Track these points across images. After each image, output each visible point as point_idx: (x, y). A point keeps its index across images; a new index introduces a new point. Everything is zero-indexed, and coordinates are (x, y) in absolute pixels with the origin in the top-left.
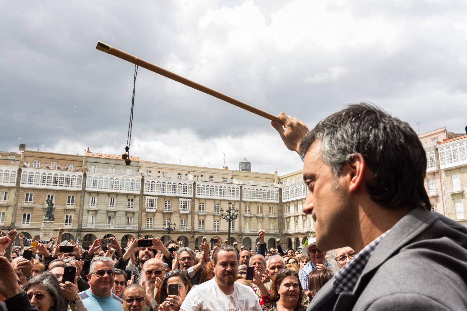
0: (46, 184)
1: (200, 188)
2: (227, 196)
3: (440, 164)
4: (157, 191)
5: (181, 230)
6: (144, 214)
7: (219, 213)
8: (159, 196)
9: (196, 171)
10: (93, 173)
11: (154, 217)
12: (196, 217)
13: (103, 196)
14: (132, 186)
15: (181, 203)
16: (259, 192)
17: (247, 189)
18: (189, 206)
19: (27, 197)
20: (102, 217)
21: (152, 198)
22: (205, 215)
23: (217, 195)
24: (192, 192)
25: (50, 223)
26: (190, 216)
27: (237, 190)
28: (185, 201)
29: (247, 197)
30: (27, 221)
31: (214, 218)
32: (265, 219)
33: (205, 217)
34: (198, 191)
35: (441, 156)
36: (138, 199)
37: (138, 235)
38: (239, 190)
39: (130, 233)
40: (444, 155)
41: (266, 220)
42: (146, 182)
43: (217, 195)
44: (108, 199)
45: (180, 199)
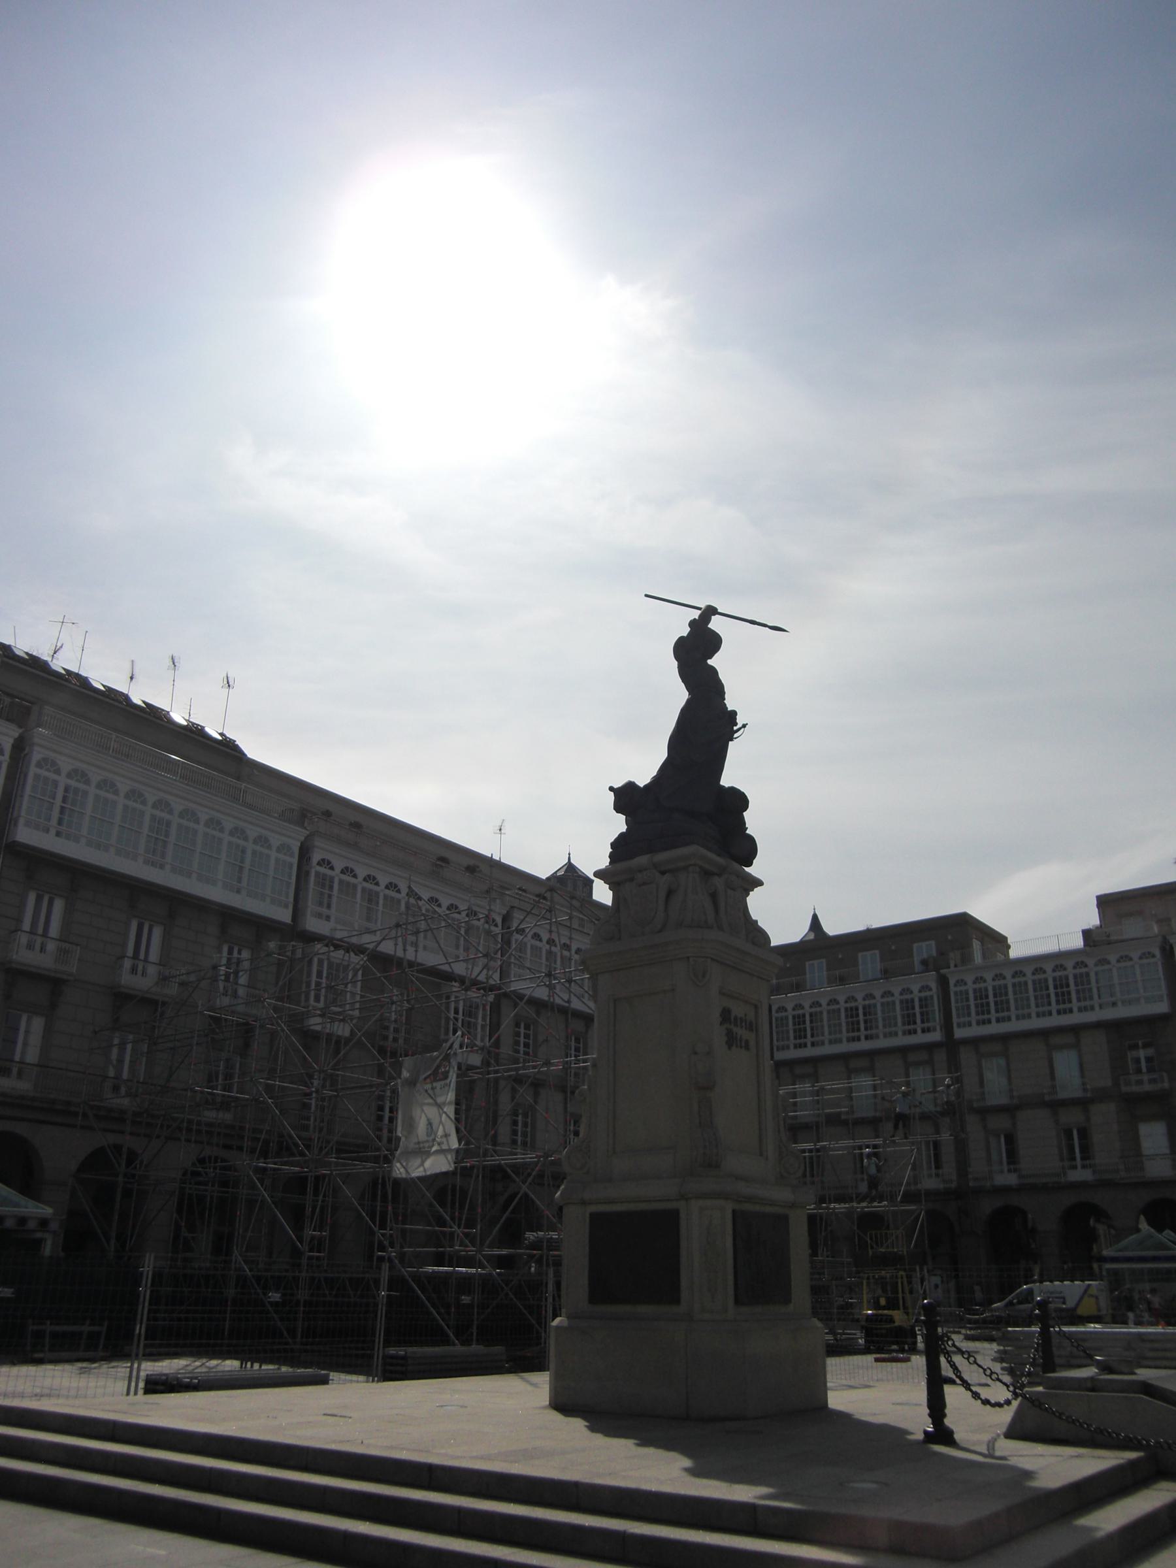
30: (1083, 1159)
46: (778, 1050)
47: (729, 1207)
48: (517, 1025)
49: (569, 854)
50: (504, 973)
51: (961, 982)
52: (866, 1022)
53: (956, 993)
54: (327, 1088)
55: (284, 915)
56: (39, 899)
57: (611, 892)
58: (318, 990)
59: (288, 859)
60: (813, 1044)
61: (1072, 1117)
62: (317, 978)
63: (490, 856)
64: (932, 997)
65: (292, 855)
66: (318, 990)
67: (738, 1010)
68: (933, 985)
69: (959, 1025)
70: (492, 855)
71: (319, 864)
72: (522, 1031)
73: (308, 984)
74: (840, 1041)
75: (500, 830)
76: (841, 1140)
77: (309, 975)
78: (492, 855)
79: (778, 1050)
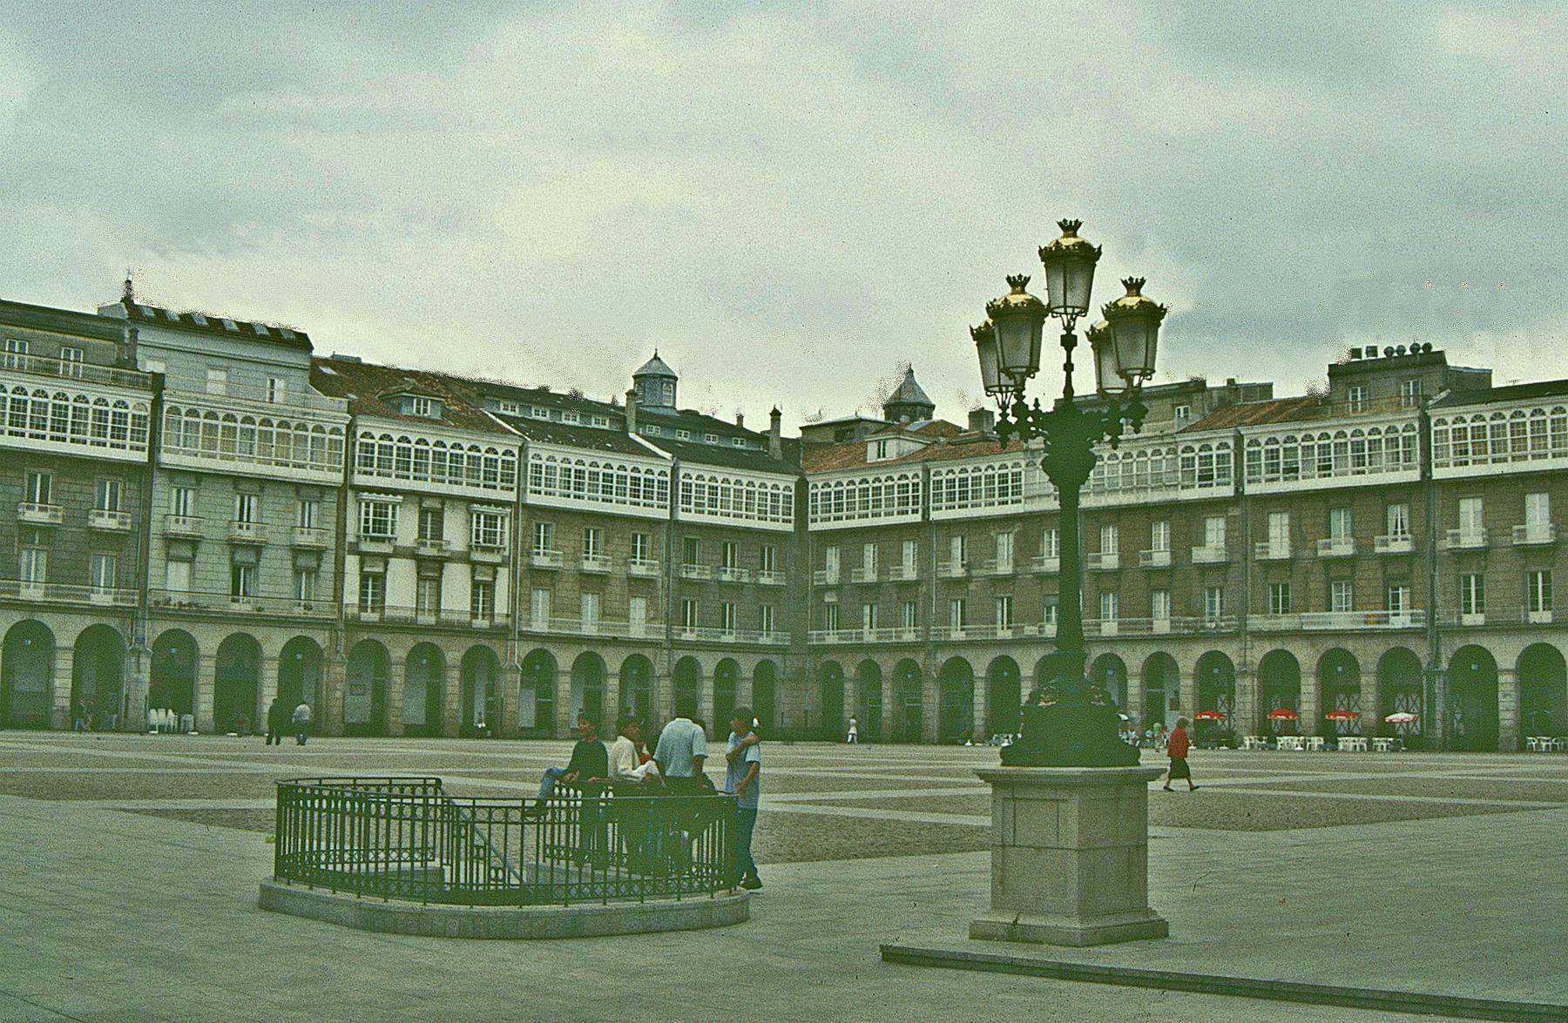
0: (412, 473)
1: (570, 470)
2: (68, 440)
3: (1433, 466)
4: (12, 428)
7: (59, 514)
12: (352, 562)
13: (217, 486)
16: (70, 408)
17: (544, 460)
19: (45, 486)
20: (216, 568)
21: (492, 510)
22: (385, 558)
23: (120, 442)
24: (144, 441)
27: (661, 478)
28: (381, 505)
32: (394, 563)
35: (1436, 442)
36: (331, 500)
38: (668, 479)
40: (1447, 438)
42: (362, 436)
43: (120, 442)
44: (170, 493)
45: (476, 507)
46: (1436, 467)
51: (1442, 422)
52: (1554, 437)
54: (349, 699)
56: (179, 492)
57: (759, 432)
63: (734, 422)
64: (1229, 454)
68: (1231, 443)
69: (933, 509)
70: (740, 418)
76: (607, 844)
78: (740, 418)
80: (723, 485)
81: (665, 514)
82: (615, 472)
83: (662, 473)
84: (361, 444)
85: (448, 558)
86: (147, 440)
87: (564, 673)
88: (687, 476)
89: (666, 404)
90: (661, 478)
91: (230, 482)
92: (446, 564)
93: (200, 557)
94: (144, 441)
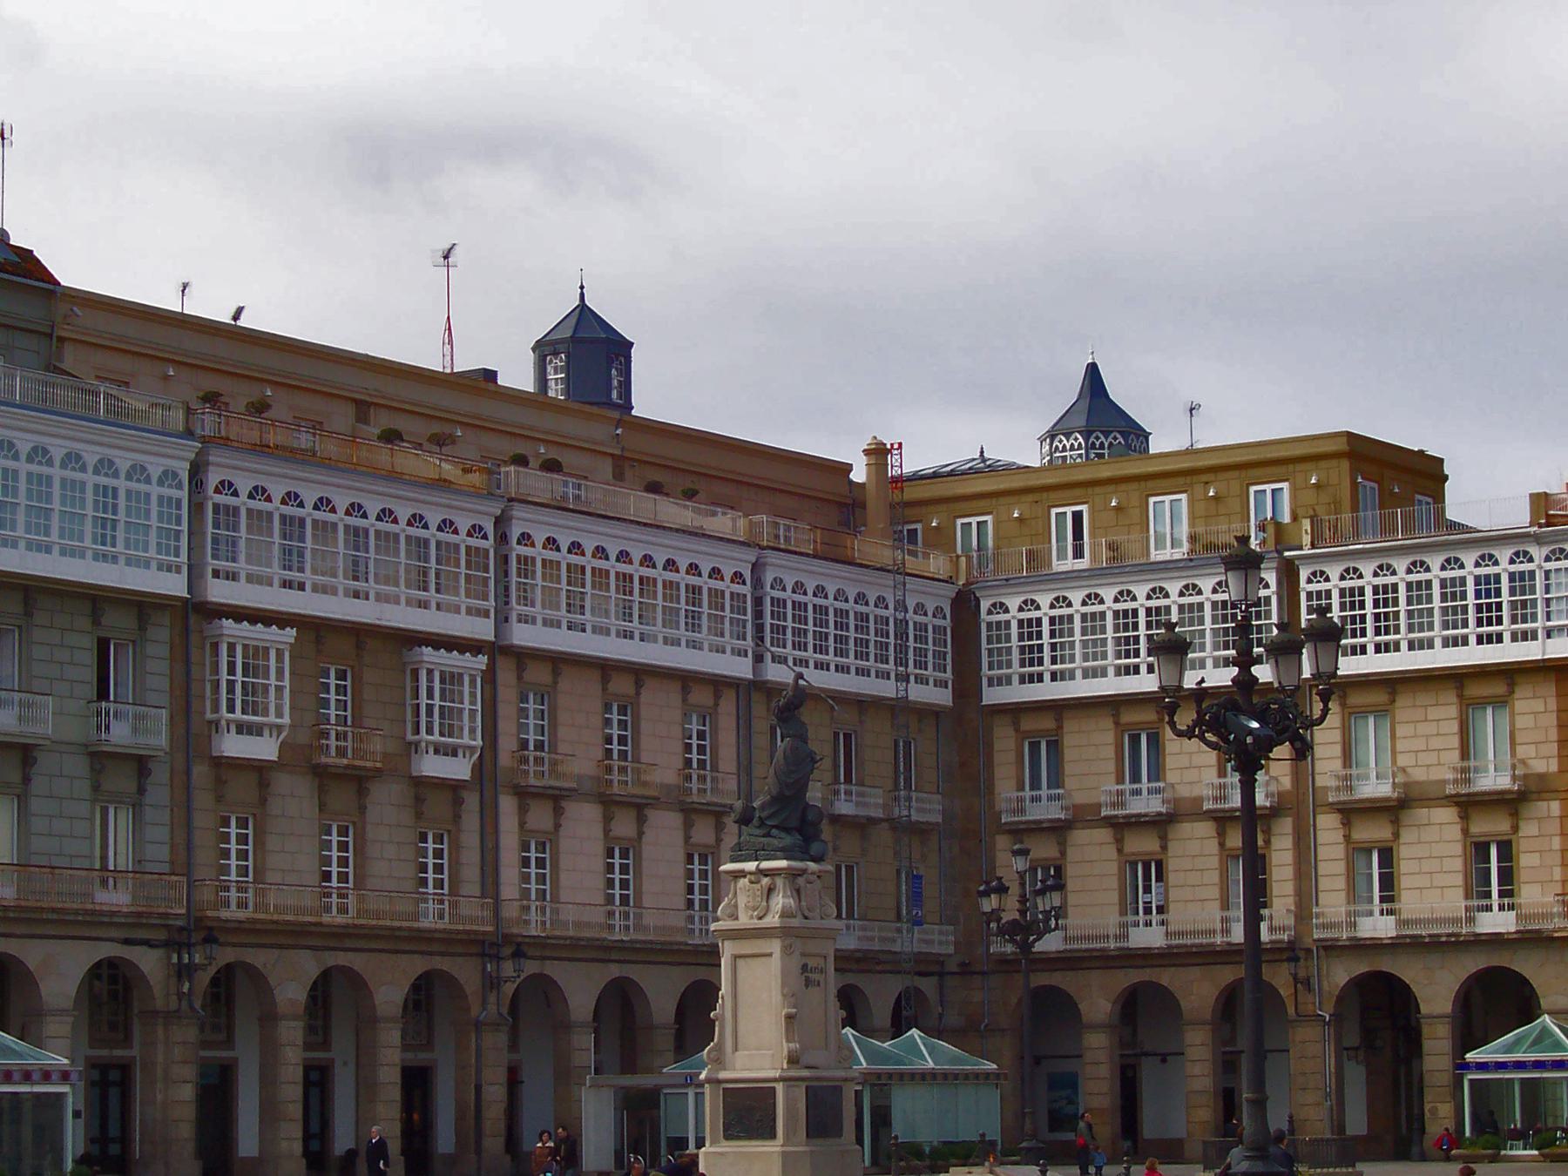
5: (326, 919)
6: (200, 771)
8: (313, 629)
9: (531, 428)
10: (1532, 724)
11: (263, 801)
14: (690, 621)
15: (232, 671)
18: (279, 689)
25: (765, 881)
26: (472, 801)
29: (308, 577)
30: (1501, 894)
31: (1119, 841)
32: (573, 809)
33: (1164, 839)
34: (414, 575)
36: (161, 635)
37: (175, 959)
38: (489, 544)
39: (127, 942)
41: (883, 835)
46: (990, 684)
47: (803, 1085)
48: (610, 854)
49: (582, 287)
50: (502, 619)
53: (1309, 595)
55: (174, 585)
58: (231, 690)
59: (175, 493)
60: (1054, 677)
61: (1491, 825)
62: (229, 674)
65: (180, 486)
66: (231, 690)
67: (812, 963)
71: (217, 491)
72: (617, 861)
73: (216, 685)
74: (1103, 673)
75: (446, 257)
77: (216, 671)
79: (990, 684)
80: (253, 504)
81: (742, 668)
82: (432, 534)
83: (475, 530)
84: (216, 507)
85: (378, 770)
86: (949, 668)
87: (1093, 1027)
88: (226, 486)
89: (1156, 555)
90: (475, 542)
91: (596, 675)
92: (564, 804)
93: (39, 785)
94: (486, 599)
